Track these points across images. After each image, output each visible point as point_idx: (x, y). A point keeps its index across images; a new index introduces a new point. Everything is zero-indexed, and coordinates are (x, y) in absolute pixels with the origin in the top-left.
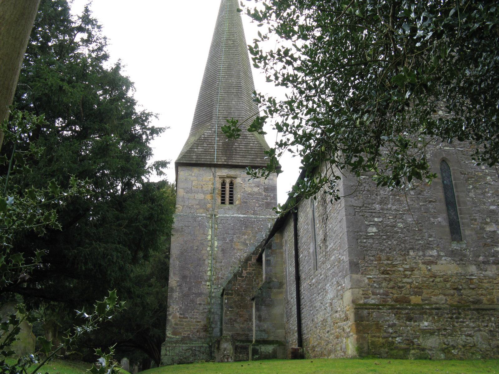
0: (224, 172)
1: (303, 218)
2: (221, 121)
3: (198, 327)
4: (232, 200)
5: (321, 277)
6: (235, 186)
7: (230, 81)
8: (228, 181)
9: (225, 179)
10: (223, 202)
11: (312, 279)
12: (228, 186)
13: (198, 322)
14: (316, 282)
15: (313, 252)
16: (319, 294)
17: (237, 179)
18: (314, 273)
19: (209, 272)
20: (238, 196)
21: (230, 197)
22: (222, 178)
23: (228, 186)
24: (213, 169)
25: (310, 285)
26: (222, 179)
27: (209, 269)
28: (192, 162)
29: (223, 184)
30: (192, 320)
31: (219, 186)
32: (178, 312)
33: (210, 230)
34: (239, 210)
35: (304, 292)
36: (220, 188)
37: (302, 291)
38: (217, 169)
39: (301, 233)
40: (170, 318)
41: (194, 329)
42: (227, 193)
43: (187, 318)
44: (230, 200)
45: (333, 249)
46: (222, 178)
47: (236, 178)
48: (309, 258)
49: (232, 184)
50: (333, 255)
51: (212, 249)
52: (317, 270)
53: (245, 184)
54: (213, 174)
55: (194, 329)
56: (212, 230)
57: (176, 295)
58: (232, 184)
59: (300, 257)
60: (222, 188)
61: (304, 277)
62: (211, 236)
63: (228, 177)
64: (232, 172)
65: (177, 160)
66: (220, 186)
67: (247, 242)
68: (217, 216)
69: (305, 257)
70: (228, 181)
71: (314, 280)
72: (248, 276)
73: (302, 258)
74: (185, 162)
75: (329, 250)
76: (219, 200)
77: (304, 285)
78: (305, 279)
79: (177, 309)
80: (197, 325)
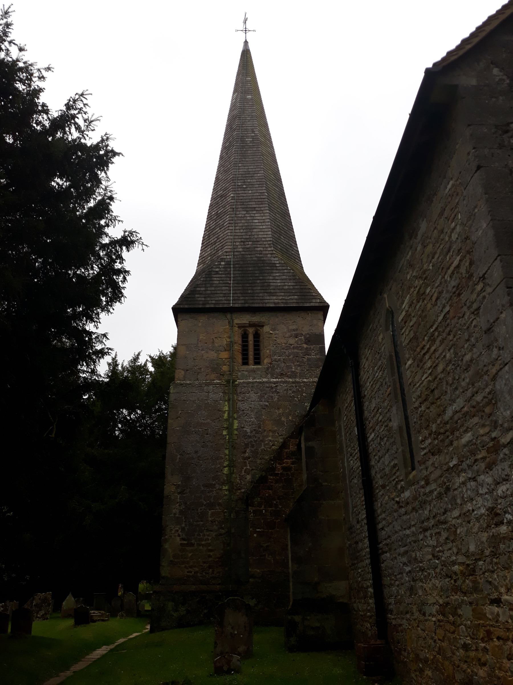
0: (245, 319)
1: (370, 358)
2: (239, 247)
3: (210, 559)
4: (259, 359)
5: (428, 490)
6: (261, 338)
7: (250, 192)
8: (251, 330)
9: (248, 329)
10: (245, 362)
11: (403, 490)
12: (251, 338)
13: (211, 551)
14: (415, 498)
15: (400, 428)
16: (426, 530)
17: (264, 328)
18: (407, 474)
19: (226, 469)
20: (266, 351)
21: (255, 354)
22: (243, 327)
23: (251, 338)
24: (229, 316)
25: (398, 503)
26: (242, 329)
27: (226, 463)
28: (197, 306)
29: (245, 337)
30: (201, 547)
31: (238, 339)
32: (179, 536)
33: (226, 403)
34: (270, 371)
35: (383, 515)
36: (240, 342)
37: (379, 511)
38: (235, 315)
39: (367, 390)
40: (166, 547)
41: (204, 563)
42: (251, 349)
43: (192, 545)
44: (255, 358)
45: (465, 414)
46: (243, 327)
47: (263, 326)
48: (392, 440)
49: (257, 336)
50: (466, 431)
51: (230, 433)
52: (413, 469)
53: (278, 333)
54: (229, 322)
55: (204, 563)
56: (229, 403)
57: (175, 509)
58: (257, 336)
59: (370, 439)
60: (243, 341)
61: (381, 482)
62: (229, 414)
63: (251, 325)
64: (256, 319)
65: (176, 304)
66: (240, 339)
67: (283, 419)
68: (236, 383)
69: (382, 439)
70: (251, 330)
71: (407, 494)
72: (285, 473)
73: (373, 440)
74: (186, 306)
75: (451, 418)
76: (239, 358)
77: (383, 499)
78: (384, 487)
79: (177, 531)
80: (210, 556)
